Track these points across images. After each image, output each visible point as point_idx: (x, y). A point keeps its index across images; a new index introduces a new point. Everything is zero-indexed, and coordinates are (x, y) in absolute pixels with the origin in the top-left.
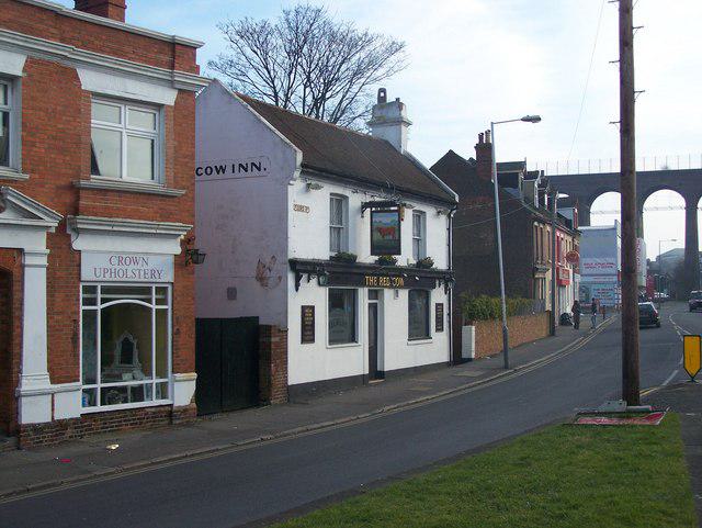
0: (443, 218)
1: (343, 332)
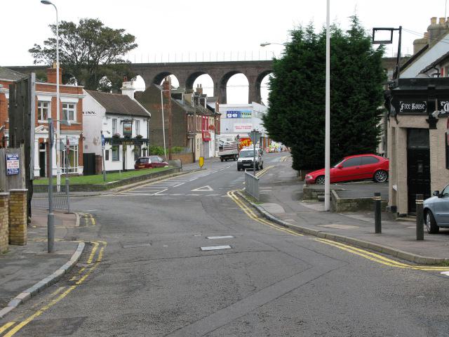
0: (146, 122)
1: (116, 159)
